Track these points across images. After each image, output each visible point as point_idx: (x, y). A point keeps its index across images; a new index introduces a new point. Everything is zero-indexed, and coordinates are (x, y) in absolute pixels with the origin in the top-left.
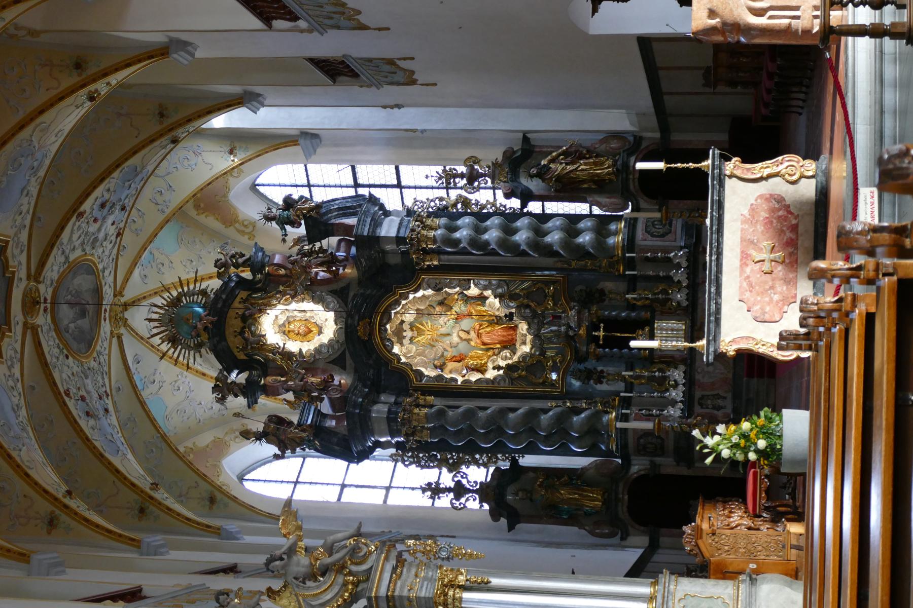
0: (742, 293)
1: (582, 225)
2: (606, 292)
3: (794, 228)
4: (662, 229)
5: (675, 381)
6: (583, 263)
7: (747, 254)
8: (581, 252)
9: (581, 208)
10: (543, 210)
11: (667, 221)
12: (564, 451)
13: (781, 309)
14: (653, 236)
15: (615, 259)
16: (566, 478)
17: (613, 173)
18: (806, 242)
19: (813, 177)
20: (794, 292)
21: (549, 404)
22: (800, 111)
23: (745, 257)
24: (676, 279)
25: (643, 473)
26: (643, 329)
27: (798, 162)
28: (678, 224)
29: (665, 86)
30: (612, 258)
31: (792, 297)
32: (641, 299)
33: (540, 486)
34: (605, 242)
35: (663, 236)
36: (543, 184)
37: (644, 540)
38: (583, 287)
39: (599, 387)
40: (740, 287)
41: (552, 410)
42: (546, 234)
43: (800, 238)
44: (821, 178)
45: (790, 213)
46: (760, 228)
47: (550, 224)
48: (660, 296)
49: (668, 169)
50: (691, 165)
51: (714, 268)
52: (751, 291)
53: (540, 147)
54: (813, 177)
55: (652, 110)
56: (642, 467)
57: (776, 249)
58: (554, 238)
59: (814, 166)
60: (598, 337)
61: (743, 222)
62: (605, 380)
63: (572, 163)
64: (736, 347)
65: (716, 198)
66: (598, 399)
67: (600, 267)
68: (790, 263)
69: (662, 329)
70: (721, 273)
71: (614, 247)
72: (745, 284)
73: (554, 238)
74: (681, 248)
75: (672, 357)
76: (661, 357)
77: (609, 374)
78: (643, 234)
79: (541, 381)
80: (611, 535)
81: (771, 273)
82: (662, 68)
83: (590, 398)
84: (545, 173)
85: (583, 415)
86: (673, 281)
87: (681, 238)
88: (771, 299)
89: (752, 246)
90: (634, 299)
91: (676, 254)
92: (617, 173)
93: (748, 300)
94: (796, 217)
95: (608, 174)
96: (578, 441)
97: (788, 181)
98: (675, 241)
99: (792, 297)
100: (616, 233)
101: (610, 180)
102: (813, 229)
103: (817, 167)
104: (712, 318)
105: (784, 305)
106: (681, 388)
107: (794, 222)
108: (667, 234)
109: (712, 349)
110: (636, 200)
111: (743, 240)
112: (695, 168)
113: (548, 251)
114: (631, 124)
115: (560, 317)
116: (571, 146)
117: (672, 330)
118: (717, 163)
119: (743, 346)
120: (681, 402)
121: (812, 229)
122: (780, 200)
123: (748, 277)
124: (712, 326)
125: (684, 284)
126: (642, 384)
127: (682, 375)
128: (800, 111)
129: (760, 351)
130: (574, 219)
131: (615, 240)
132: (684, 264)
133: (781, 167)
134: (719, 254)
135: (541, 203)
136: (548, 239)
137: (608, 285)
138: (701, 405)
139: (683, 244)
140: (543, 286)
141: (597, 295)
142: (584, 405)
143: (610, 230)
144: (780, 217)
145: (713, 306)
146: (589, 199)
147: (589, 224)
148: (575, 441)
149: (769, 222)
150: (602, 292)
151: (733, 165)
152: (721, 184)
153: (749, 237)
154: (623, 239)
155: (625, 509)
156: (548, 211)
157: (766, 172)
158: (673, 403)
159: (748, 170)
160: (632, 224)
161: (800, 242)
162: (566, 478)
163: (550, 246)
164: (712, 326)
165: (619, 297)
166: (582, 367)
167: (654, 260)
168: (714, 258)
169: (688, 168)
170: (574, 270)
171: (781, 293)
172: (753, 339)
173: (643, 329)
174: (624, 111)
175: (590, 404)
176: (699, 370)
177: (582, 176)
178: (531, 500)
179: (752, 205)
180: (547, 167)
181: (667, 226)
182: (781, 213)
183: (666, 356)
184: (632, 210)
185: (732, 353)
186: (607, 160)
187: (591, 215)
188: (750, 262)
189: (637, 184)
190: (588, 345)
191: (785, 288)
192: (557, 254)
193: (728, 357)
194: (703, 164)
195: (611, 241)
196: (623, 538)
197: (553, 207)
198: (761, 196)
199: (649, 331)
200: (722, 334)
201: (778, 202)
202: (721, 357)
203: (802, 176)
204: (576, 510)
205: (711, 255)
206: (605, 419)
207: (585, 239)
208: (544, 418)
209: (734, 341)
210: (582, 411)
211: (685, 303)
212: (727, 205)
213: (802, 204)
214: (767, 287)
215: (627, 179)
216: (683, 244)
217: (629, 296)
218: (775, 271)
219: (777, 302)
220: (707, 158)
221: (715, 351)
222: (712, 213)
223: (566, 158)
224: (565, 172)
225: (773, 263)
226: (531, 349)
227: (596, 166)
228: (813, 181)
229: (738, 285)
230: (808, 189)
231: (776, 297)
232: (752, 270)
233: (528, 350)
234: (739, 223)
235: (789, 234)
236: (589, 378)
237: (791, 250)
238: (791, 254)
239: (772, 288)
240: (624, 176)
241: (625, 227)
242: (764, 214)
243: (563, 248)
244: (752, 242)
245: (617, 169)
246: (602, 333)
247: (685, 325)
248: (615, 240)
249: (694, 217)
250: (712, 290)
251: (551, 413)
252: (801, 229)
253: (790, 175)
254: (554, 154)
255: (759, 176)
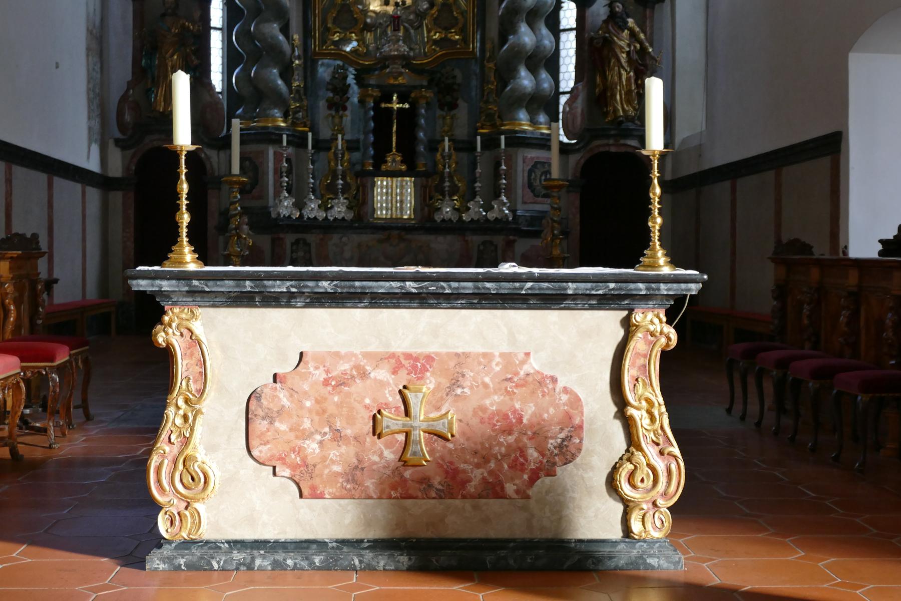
0: (320, 360)
1: (544, 75)
2: (453, 112)
3: (493, 489)
4: (539, 185)
5: (332, 207)
6: (492, 79)
7: (424, 369)
8: (506, 74)
9: (568, 77)
10: (565, 30)
11: (549, 190)
12: (231, 59)
13: (282, 459)
14: (530, 172)
15: (498, 122)
16: (196, 62)
17: (616, 117)
18: (460, 521)
19: (627, 531)
20: (328, 491)
21: (296, 37)
22: (738, 408)
23: (417, 364)
24: (471, 205)
25: (208, 166)
26: (402, 162)
27: (665, 494)
28: (543, 206)
29: (747, 183)
30: (499, 117)
31: (313, 488)
32: (443, 157)
33: (183, 26)
34: (520, 107)
35: (530, 185)
36: (600, 23)
37: (116, 170)
38: (459, 78)
39: (322, 104)
40: (337, 355)
41: (291, 43)
42: (531, 25)
43: (468, 504)
44: (624, 555)
45: (534, 477)
46: (494, 402)
47: (545, 31)
48: (447, 184)
49: (648, 160)
50: (656, 222)
51: (383, 287)
52: (326, 383)
53: (652, 17)
54: (627, 531)
55: (707, 166)
56: (215, 165)
57: (439, 444)
58: (526, 36)
59: (657, 535)
60: (390, 101)
61: (507, 357)
62: (333, 113)
63: (630, 60)
64: (179, 345)
65: (571, 288)
66: (305, 103)
67: (487, 102)
68: (404, 481)
69: (402, 187)
70: (372, 305)
71: (514, 120)
72: (345, 366)
73: (526, 36)
74: (513, 211)
75: (364, 202)
76: (364, 186)
77: (341, 117)
78: (532, 158)
79: (330, 25)
80: (121, 126)
81: (376, 432)
82: (733, 190)
83: (309, 90)
84: (616, 24)
85: (280, 82)
86: (469, 201)
87: (527, 211)
88: (306, 435)
89: (445, 383)
90: (444, 150)
91: (504, 204)
92: (617, 123)
93: (305, 377)
94: (523, 494)
95: (615, 110)
96: (245, 76)
97: (615, 469)
98: (524, 203)
99: (313, 488)
100: (533, 122)
101: (607, 113)
102: (492, 534)
103: (653, 542)
104: (248, 285)
105: (294, 467)
106: (321, 215)
107: (510, 488)
108: (533, 191)
109: (166, 285)
110: (578, 151)
111: (461, 358)
112: (648, 231)
113: (507, 28)
114: (684, 141)
115: (396, 29)
116: (653, 58)
117: (402, 202)
118: (664, 288)
119: (183, 366)
120: (301, 216)
121: (493, 533)
122: (567, 452)
123: (364, 375)
124: (228, 285)
125: (465, 217)
126: (329, 163)
127: (340, 217)
128: (738, 408)
129: (170, 411)
130: (552, 64)
131: (523, 121)
132: (491, 216)
133: (651, 451)
134: (422, 300)
135: (575, 26)
136: (524, 28)
137: (462, 112)
138: (297, 242)
139: (519, 213)
140: (460, 25)
141: (448, 99)
142: (296, 84)
143: (537, 114)
144: (522, 451)
145: (280, 287)
146: (580, 86)
147: (546, 85)
148: (246, 71)
149: (509, 424)
150: (453, 106)
151: (656, 329)
152: (605, 302)
153: (469, 374)
154: (524, 131)
155: (156, 144)
156: (563, 36)
157: (638, 415)
158: (300, 205)
159: (646, 369)
160: (544, 143)
161: (458, 502)
162: (196, 62)
163: (514, 30)
164: (228, 285)
165: (446, 128)
166: (351, 80)
167: (497, 175)
168: (411, 286)
169: (649, 212)
170: (482, 67)
171: (324, 459)
172: (202, 392)
173: (402, 162)
174: (704, 128)
175: (298, 91)
176: (344, 239)
177: (612, 76)
178: (163, 15)
179: (554, 380)
180: (623, 26)
181: (544, 192)
182: (532, 454)
183: (365, 194)
184: (561, 143)
185: (161, 339)
186: (634, 108)
187: (558, 94)
188: (403, 378)
189: (602, 149)
190: (378, 86)
191: (337, 468)
192: (503, 39)
193: (153, 326)
194: (660, 253)
195: (523, 115)
196: (117, 142)
197: (569, 45)
198: (576, 402)
199: (401, 170)
200: (211, 311)
201: (560, 447)
202: (151, 310)
203: (628, 507)
204: (153, 79)
205: (416, 278)
206: (277, 113)
207: (525, 80)
208: (274, 29)
209: (195, 341)
210: (287, 80)
211: (438, 218)
212: (552, 317)
213: (558, 507)
214: (338, 425)
215: (608, 137)
216: (519, 213)
217: (447, 143)
218: (380, 443)
219: (299, 451)
220: (675, 262)
221: (166, 295)
222: (531, 278)
223: (637, 52)
224: (618, 51)
225: (401, 438)
226: (374, 12)
227: (626, 94)
228: (616, 533)
229: (343, 351)
230: (595, 519)
231: (312, 447)
232: (382, 384)
233: (372, 8)
234: (505, 348)
235: (477, 475)
236: (334, 90)
237: (436, 481)
238: (425, 481)
239: (338, 436)
240: (612, 132)
241: (542, 134)
242: (529, 412)
243: (512, 47)
244: (455, 383)
245: (621, 123)
246: (396, 106)
247: (409, 219)
248: (523, 121)
249: (553, 229)
250: (325, 285)
251: (281, 37)
252: (493, 505)
253: (632, 475)
254: (642, 36)
255: (630, 396)
